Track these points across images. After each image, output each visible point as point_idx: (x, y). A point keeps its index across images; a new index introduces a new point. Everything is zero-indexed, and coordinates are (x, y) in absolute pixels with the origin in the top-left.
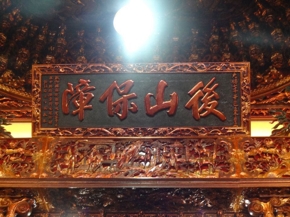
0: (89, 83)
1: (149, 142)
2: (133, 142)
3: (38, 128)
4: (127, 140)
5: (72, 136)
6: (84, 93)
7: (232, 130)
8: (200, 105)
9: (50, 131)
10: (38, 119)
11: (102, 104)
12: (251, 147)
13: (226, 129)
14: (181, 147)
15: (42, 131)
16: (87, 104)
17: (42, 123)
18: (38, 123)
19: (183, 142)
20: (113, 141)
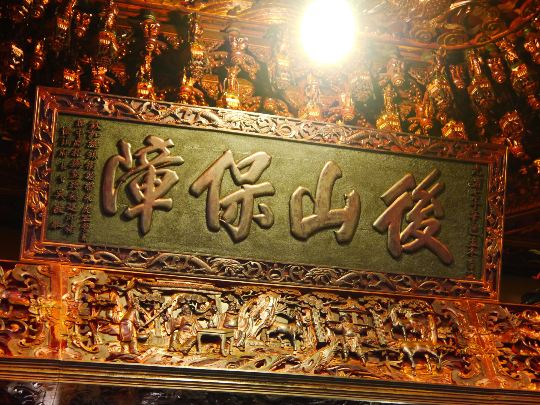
0: (170, 147)
1: (293, 295)
2: (259, 292)
3: (39, 239)
4: (245, 287)
5: (119, 265)
6: (156, 169)
7: (463, 284)
8: (404, 224)
9: (69, 249)
10: (40, 219)
11: (197, 199)
12: (501, 324)
13: (453, 282)
14: (362, 314)
15: (47, 247)
16: (162, 197)
17: (50, 228)
18: (40, 227)
19: (366, 302)
20: (214, 285)
